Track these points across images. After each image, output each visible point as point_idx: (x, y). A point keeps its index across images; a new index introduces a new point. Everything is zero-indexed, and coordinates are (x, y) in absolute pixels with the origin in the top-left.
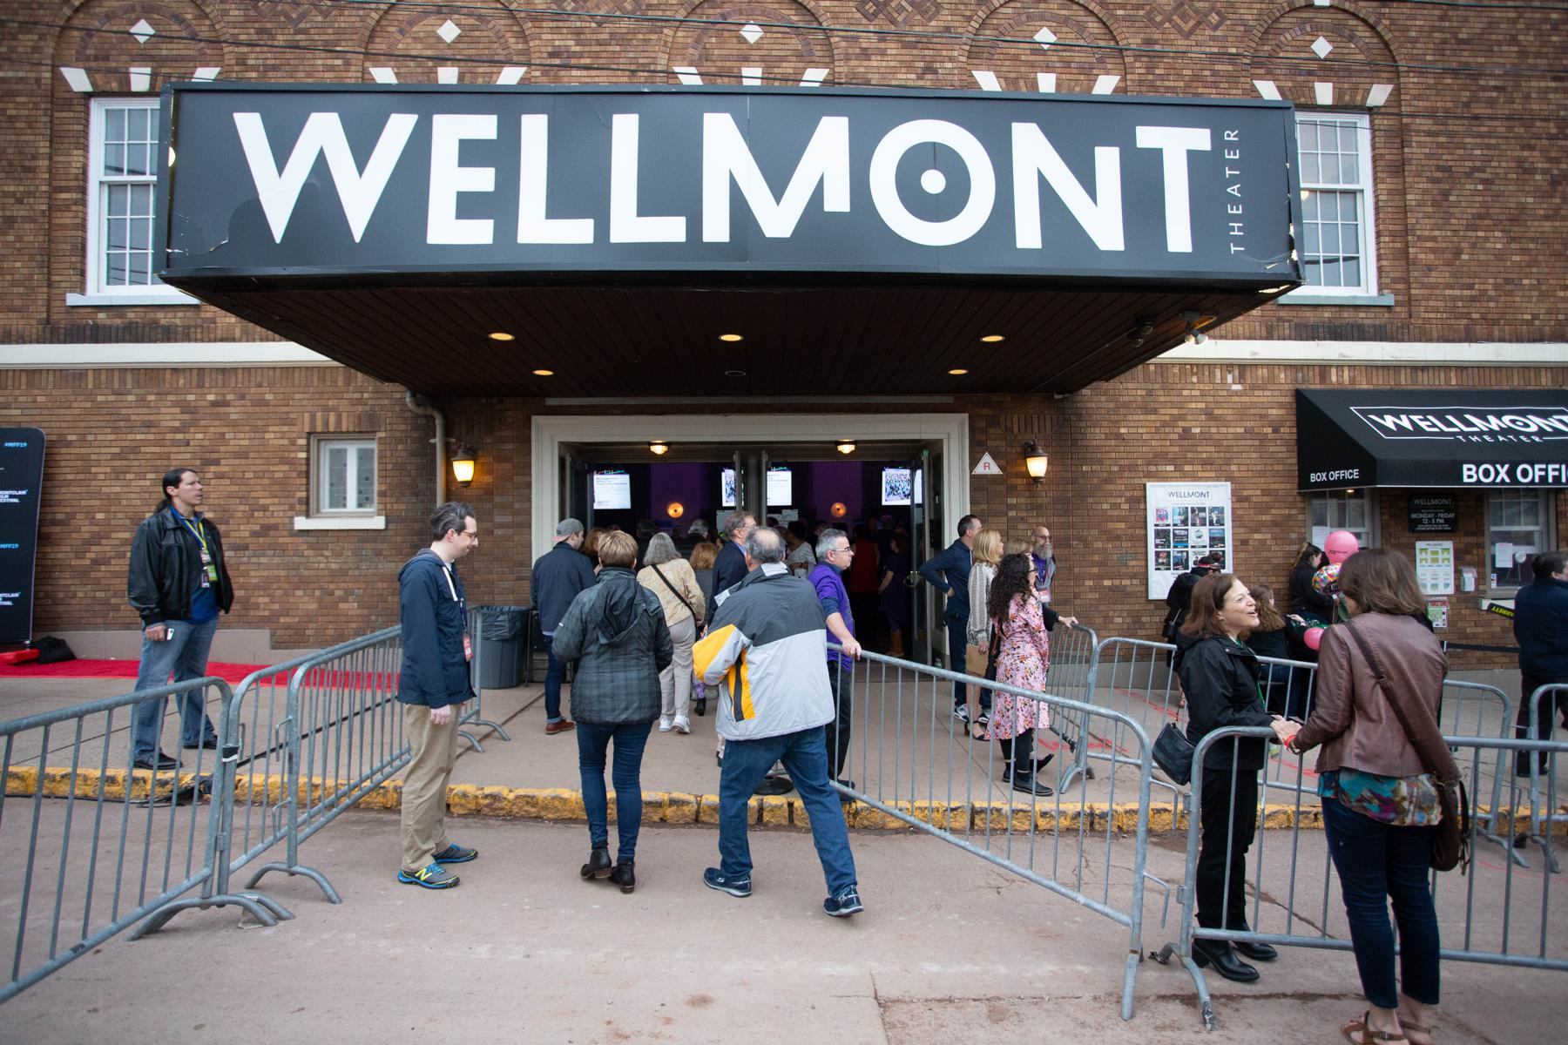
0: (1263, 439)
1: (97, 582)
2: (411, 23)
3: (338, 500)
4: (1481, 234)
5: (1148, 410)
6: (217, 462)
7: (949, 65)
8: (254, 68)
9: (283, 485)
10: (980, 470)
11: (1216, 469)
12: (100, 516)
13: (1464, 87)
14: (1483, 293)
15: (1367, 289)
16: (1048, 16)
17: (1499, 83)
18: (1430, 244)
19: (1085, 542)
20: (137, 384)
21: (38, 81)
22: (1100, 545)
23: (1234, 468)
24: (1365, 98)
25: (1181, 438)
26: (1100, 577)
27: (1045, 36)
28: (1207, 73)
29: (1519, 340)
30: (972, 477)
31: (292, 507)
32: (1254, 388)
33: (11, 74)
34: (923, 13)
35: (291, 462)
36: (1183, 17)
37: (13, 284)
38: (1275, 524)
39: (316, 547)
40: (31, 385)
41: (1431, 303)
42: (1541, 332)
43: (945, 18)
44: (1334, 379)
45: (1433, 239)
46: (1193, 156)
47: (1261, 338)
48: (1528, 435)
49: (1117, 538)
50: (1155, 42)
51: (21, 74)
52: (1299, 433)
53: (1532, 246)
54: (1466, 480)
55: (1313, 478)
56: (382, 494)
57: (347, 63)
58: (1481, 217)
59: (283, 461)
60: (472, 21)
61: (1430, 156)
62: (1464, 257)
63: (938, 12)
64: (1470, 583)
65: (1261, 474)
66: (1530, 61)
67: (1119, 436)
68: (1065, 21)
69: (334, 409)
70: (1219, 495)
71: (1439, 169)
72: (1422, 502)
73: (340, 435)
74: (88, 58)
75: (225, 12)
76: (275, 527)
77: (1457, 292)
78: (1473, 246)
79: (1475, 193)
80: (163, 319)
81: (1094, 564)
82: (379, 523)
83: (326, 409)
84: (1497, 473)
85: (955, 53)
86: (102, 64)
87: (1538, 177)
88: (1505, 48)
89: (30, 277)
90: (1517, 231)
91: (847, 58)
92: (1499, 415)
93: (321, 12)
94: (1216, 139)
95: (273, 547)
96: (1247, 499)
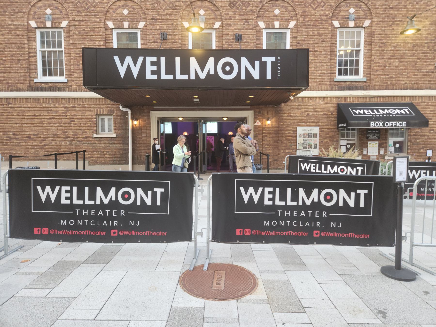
0: (328, 116)
1: (45, 150)
2: (116, 10)
3: (103, 130)
4: (392, 61)
5: (298, 109)
6: (74, 121)
7: (251, 20)
8: (77, 21)
9: (90, 127)
10: (256, 124)
11: (316, 123)
12: (45, 134)
13: (391, 21)
14: (392, 77)
15: (361, 77)
16: (278, 5)
17: (400, 19)
18: (377, 64)
19: (282, 141)
20: (53, 102)
21: (24, 25)
22: (285, 142)
23: (320, 123)
24: (363, 24)
25: (307, 116)
26: (285, 150)
27: (277, 12)
28: (319, 20)
29: (401, 89)
30: (254, 126)
31: (93, 132)
32: (327, 103)
33: (17, 23)
34: (245, 6)
35: (92, 121)
36: (314, 4)
37: (21, 77)
38: (330, 137)
39: (99, 142)
40: (27, 102)
41: (377, 80)
42: (407, 87)
43: (251, 7)
44: (348, 100)
45: (379, 63)
46: (272, 62)
47: (329, 90)
48: (392, 114)
49: (290, 140)
50: (306, 12)
51: (19, 23)
52: (338, 114)
53: (406, 64)
54: (371, 126)
55: (340, 125)
56: (115, 129)
57: (101, 20)
58: (393, 56)
59: (90, 121)
60: (131, 9)
61: (380, 40)
62: (387, 67)
63: (249, 6)
64: (382, 152)
65: (327, 125)
66: (410, 13)
67: (291, 116)
68: (282, 7)
69: (102, 108)
70: (316, 130)
71: (382, 43)
72: (371, 131)
73: (104, 115)
74: (35, 19)
75: (69, 7)
76: (89, 137)
77: (384, 77)
78: (390, 64)
79: (391, 50)
80: (58, 85)
81: (284, 146)
82: (114, 136)
83: (100, 108)
84: (380, 124)
85: (253, 17)
86: (39, 20)
87: (409, 45)
88: (403, 9)
89: (25, 75)
90: (402, 60)
91: (226, 19)
92: (388, 109)
93: (93, 6)
94: (276, 59)
95: (88, 141)
96: (323, 131)
